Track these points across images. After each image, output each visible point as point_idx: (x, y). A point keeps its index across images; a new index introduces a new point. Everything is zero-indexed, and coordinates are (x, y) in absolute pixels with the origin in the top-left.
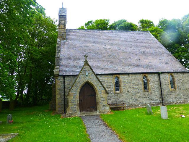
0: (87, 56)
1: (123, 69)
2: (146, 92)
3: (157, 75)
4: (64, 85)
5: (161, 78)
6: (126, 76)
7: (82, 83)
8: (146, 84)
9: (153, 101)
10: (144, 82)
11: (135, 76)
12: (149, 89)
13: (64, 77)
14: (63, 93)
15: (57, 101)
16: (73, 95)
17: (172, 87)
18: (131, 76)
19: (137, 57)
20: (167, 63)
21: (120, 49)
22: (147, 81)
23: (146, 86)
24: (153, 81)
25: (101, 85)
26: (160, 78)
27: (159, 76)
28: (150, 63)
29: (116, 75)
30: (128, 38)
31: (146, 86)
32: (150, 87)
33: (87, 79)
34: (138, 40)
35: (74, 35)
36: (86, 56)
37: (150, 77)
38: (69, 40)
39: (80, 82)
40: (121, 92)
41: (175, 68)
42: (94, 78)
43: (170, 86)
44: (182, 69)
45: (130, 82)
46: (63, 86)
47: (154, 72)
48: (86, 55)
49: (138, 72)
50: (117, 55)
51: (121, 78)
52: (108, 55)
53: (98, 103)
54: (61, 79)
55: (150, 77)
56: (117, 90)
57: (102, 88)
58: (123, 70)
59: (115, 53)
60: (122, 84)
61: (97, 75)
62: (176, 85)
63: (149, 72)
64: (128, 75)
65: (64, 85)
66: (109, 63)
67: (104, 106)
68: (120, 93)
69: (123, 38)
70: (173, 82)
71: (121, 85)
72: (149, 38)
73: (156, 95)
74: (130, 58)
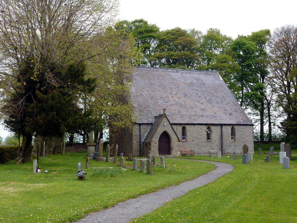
0: (165, 110)
1: (190, 119)
2: (208, 142)
3: (219, 127)
4: (140, 132)
5: (223, 129)
6: (193, 126)
7: (161, 132)
8: (209, 135)
9: (214, 151)
10: (208, 133)
11: (200, 127)
12: (211, 139)
13: (140, 125)
14: (139, 139)
15: (134, 146)
16: (154, 142)
17: (232, 138)
18: (196, 126)
19: (202, 107)
20: (231, 114)
21: (186, 96)
22: (210, 132)
23: (209, 137)
24: (215, 131)
25: (175, 135)
26: (222, 129)
27: (222, 127)
28: (215, 113)
29: (183, 125)
30: (195, 81)
31: (209, 137)
32: (212, 137)
33: (165, 129)
34: (204, 84)
35: (138, 75)
36: (164, 110)
37: (213, 128)
38: (134, 82)
39: (160, 131)
40: (186, 141)
41: (238, 121)
42: (170, 127)
43: (230, 137)
44: (245, 121)
45: (195, 131)
46: (139, 133)
47: (217, 123)
48: (164, 109)
49: (203, 123)
50: (183, 104)
51: (235, 127)
52: (174, 102)
53: (172, 148)
54: (137, 127)
55: (213, 128)
56: (208, 139)
57: (176, 137)
58: (190, 120)
59: (181, 101)
60: (188, 134)
61: (172, 124)
62: (236, 137)
63: (213, 123)
64: (194, 125)
65: (140, 132)
66: (176, 112)
67: (177, 151)
68: (185, 142)
69: (189, 81)
70: (233, 133)
71: (188, 135)
72: (217, 82)
73: (217, 145)
74: (196, 107)
